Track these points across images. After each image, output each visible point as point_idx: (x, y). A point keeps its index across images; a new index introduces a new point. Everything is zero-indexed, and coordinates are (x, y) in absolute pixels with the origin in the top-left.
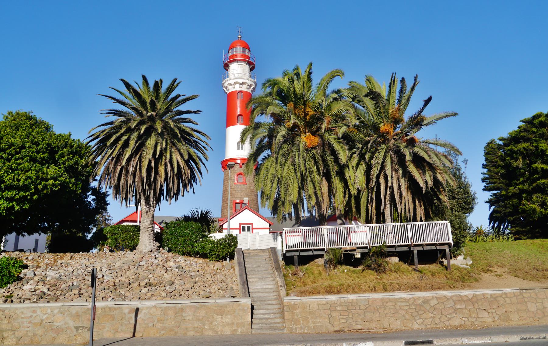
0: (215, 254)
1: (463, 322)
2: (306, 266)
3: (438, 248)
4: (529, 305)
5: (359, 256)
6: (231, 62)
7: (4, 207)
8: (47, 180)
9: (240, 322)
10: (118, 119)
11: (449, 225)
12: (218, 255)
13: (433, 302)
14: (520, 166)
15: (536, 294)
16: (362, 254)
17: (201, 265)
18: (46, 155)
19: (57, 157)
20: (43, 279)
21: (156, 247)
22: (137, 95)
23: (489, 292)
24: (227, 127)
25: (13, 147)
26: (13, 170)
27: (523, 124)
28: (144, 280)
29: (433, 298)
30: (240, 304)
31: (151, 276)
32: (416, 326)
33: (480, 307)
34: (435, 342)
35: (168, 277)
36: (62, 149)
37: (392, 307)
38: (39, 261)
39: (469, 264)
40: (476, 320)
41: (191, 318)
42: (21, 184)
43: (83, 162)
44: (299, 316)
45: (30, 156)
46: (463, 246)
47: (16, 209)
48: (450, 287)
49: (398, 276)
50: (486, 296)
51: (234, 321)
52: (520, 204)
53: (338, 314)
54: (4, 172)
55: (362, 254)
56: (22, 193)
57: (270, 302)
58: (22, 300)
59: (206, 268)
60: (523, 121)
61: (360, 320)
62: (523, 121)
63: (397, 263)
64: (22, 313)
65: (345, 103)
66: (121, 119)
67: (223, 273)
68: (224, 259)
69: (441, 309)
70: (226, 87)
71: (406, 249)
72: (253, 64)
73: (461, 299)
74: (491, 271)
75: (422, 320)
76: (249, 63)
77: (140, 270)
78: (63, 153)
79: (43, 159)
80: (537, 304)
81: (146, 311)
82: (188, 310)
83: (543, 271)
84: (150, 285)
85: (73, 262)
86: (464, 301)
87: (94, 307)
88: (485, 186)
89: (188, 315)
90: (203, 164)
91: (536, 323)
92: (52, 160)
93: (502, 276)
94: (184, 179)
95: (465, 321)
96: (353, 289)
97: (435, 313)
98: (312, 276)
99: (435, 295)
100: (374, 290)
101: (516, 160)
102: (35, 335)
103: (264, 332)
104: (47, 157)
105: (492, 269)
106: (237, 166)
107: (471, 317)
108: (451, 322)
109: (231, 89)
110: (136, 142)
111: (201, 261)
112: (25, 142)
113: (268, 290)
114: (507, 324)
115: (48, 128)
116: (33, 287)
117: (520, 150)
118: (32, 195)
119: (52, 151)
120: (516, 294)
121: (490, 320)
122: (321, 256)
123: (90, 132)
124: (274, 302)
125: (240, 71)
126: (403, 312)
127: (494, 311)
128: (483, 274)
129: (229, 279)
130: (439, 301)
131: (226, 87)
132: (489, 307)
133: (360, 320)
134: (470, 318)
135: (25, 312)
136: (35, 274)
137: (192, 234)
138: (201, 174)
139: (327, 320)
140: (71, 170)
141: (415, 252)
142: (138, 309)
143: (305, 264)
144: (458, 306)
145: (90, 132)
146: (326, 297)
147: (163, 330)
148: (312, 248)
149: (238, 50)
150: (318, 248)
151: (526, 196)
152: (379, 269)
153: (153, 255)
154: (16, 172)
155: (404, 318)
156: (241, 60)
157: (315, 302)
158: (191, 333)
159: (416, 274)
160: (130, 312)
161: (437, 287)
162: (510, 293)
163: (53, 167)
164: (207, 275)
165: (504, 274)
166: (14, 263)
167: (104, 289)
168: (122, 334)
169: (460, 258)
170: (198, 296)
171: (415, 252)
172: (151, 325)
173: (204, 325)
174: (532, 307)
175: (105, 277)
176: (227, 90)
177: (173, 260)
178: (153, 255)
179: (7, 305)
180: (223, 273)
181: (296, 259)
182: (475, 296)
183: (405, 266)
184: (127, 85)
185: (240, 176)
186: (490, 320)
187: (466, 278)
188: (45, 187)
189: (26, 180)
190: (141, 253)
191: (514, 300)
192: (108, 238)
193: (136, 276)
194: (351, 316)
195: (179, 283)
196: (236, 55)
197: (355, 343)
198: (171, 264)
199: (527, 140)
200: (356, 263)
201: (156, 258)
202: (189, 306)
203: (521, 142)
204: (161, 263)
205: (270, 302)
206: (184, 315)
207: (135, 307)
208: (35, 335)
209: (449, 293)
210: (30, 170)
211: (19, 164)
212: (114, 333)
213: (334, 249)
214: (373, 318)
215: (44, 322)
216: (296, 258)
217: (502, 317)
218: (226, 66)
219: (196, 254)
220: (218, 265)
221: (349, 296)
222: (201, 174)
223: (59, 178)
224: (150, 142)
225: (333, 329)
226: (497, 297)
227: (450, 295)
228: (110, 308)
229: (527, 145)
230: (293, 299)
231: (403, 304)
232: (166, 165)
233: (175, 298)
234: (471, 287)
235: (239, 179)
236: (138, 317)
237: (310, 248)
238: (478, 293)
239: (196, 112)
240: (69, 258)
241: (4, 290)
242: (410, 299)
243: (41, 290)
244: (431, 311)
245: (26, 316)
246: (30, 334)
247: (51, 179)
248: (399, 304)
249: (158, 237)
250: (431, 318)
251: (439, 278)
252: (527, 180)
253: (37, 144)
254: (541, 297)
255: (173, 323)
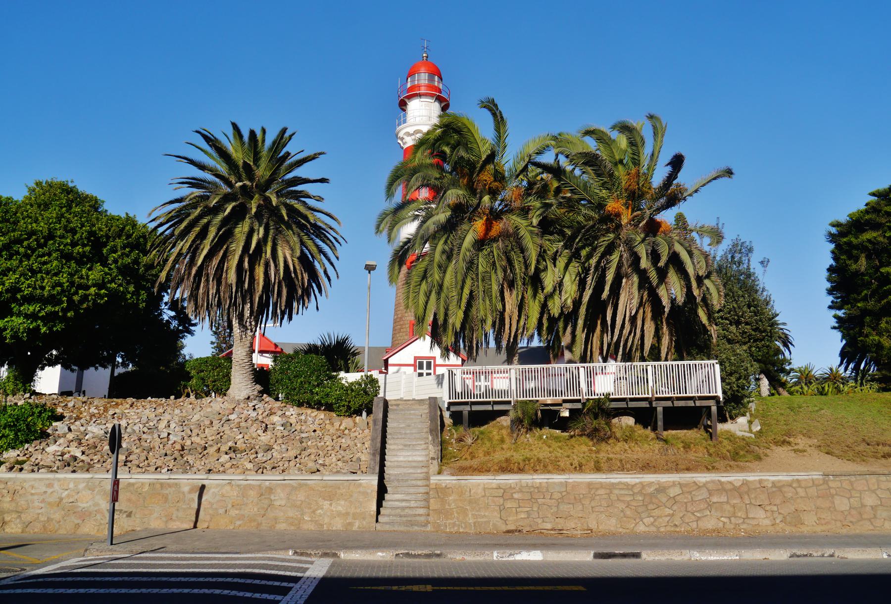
0: (344, 406)
1: (721, 525)
2: (482, 428)
3: (698, 403)
4: (837, 500)
5: (566, 414)
6: (410, 97)
7: (24, 329)
8: (87, 288)
9: (358, 511)
10: (192, 193)
11: (717, 367)
12: (349, 408)
13: (673, 492)
14: (863, 269)
15: (852, 483)
16: (571, 411)
17: (321, 422)
18: (88, 248)
19: (105, 251)
20: (80, 437)
21: (256, 393)
22: (223, 154)
23: (770, 477)
25: (34, 237)
26: (34, 272)
27: (875, 199)
28: (229, 441)
29: (674, 484)
30: (360, 485)
31: (241, 436)
32: (641, 528)
33: (753, 501)
34: (644, 555)
35: (265, 438)
36: (114, 239)
37: (606, 496)
38: (83, 409)
39: (754, 430)
40: (743, 523)
41: (283, 503)
42: (46, 294)
43: (145, 260)
44: (453, 506)
45: (62, 251)
46: (749, 402)
47: (42, 331)
48: (707, 468)
49: (627, 447)
50: (765, 484)
51: (349, 510)
52: (861, 334)
53: (515, 505)
54: (20, 276)
55: (571, 411)
56: (49, 308)
57: (414, 482)
58: (37, 467)
59: (328, 427)
60: (873, 194)
61: (549, 516)
62: (873, 194)
63: (631, 427)
64: (33, 487)
66: (197, 192)
67: (353, 435)
68: (358, 413)
69: (686, 503)
70: (402, 139)
71: (645, 404)
72: (445, 100)
73: (721, 488)
74: (789, 443)
75: (652, 519)
76: (440, 99)
77: (226, 428)
78: (115, 246)
79: (83, 255)
80: (852, 500)
81: (216, 490)
82: (279, 491)
83: (878, 445)
84: (234, 451)
85: (132, 412)
86: (726, 491)
87: (116, 482)
88: (832, 302)
89: (279, 497)
90: (332, 264)
91: (844, 531)
92: (97, 256)
93: (805, 451)
94: (298, 288)
95: (724, 523)
96: (545, 467)
97: (675, 508)
98: (488, 444)
99: (678, 479)
100: (580, 468)
101: (856, 259)
102: (49, 520)
103: (396, 528)
104: (90, 252)
105: (791, 440)
107: (736, 517)
108: (701, 524)
110: (219, 230)
111: (322, 415)
112: (56, 229)
113: (414, 464)
114: (794, 529)
115: (95, 205)
116: (61, 449)
117: (861, 244)
118: (65, 311)
119: (97, 242)
120: (816, 482)
121: (767, 522)
122: (504, 413)
123: (150, 214)
124: (420, 483)
125: (424, 112)
126: (621, 506)
127: (775, 508)
128: (774, 447)
129: (359, 445)
130: (685, 489)
131: (402, 139)
132: (767, 502)
133: (549, 516)
134: (733, 519)
135: (36, 485)
136: (70, 430)
137: (312, 373)
138: (329, 280)
139: (497, 514)
140: (129, 272)
141: (660, 410)
142: (203, 487)
143: (483, 425)
144: (715, 499)
145: (150, 214)
146: (497, 478)
147: (239, 519)
148: (491, 399)
149: (422, 78)
150: (500, 399)
151: (871, 321)
152: (595, 435)
153: (251, 404)
154: (39, 275)
155: (622, 514)
156: (426, 95)
157: (479, 485)
158: (282, 526)
159: (657, 446)
160: (191, 491)
161: (684, 467)
162: (806, 480)
163: (98, 267)
164: (327, 438)
165: (808, 449)
166: (40, 413)
167: (166, 455)
168: (178, 523)
169: (742, 420)
170: (300, 470)
171: (660, 410)
172: (221, 511)
173: (302, 514)
174: (842, 504)
175: (171, 436)
176: (404, 144)
177: (280, 413)
178: (251, 404)
179: (11, 475)
180: (353, 435)
181: (473, 416)
182: (745, 483)
183: (640, 431)
184: (207, 139)
186: (767, 522)
187: (742, 453)
188: (85, 298)
189: (53, 288)
190: (233, 400)
191: (813, 491)
192: (192, 377)
193: (219, 436)
194: (535, 509)
195: (279, 448)
196: (419, 86)
197: (512, 552)
198: (276, 419)
199: (876, 226)
200: (563, 424)
201: (254, 409)
202: (282, 485)
203: (866, 230)
204: (260, 418)
205: (414, 482)
206: (272, 497)
207: (200, 483)
208: (49, 520)
209: (702, 478)
210: (60, 272)
211: (45, 263)
212: (166, 522)
213: (525, 402)
214: (572, 513)
215: (64, 501)
216: (466, 414)
217: (788, 519)
218: (403, 105)
219: (318, 405)
220: (347, 422)
221: (535, 477)
222: (329, 280)
223: (109, 285)
224: (240, 231)
225: (504, 528)
226: (783, 486)
227: (704, 480)
228: (162, 485)
229: (875, 234)
230: (447, 479)
231: (623, 492)
232: (267, 265)
233: (265, 471)
234: (742, 469)
236: (203, 499)
237: (488, 400)
238: (751, 479)
239: (323, 181)
240: (128, 406)
241: (19, 453)
242: (635, 484)
243: (72, 453)
244: (669, 504)
245: (38, 491)
246: (42, 518)
247: (94, 285)
248: (616, 492)
249: (261, 376)
250: (669, 515)
251: (695, 452)
252: (872, 296)
253: (73, 231)
254: (859, 488)
255: (256, 509)
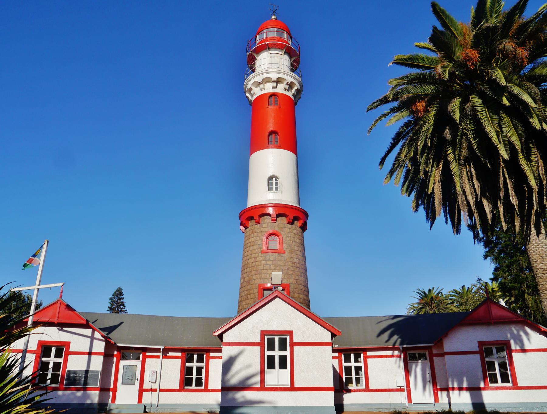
24: (252, 152)
62: (417, 207)
65: (434, 169)
76: (289, 52)
106: (267, 220)
109: (258, 92)
131: (251, 89)
185: (272, 237)
218: (251, 60)
235: (270, 243)
239: (370, 130)
